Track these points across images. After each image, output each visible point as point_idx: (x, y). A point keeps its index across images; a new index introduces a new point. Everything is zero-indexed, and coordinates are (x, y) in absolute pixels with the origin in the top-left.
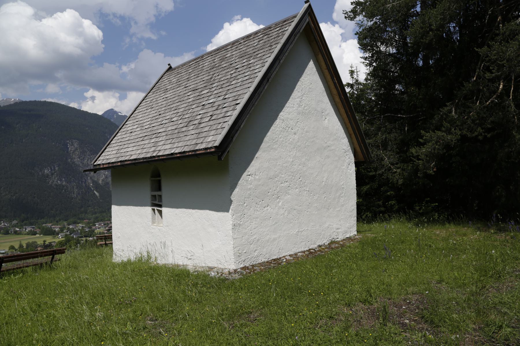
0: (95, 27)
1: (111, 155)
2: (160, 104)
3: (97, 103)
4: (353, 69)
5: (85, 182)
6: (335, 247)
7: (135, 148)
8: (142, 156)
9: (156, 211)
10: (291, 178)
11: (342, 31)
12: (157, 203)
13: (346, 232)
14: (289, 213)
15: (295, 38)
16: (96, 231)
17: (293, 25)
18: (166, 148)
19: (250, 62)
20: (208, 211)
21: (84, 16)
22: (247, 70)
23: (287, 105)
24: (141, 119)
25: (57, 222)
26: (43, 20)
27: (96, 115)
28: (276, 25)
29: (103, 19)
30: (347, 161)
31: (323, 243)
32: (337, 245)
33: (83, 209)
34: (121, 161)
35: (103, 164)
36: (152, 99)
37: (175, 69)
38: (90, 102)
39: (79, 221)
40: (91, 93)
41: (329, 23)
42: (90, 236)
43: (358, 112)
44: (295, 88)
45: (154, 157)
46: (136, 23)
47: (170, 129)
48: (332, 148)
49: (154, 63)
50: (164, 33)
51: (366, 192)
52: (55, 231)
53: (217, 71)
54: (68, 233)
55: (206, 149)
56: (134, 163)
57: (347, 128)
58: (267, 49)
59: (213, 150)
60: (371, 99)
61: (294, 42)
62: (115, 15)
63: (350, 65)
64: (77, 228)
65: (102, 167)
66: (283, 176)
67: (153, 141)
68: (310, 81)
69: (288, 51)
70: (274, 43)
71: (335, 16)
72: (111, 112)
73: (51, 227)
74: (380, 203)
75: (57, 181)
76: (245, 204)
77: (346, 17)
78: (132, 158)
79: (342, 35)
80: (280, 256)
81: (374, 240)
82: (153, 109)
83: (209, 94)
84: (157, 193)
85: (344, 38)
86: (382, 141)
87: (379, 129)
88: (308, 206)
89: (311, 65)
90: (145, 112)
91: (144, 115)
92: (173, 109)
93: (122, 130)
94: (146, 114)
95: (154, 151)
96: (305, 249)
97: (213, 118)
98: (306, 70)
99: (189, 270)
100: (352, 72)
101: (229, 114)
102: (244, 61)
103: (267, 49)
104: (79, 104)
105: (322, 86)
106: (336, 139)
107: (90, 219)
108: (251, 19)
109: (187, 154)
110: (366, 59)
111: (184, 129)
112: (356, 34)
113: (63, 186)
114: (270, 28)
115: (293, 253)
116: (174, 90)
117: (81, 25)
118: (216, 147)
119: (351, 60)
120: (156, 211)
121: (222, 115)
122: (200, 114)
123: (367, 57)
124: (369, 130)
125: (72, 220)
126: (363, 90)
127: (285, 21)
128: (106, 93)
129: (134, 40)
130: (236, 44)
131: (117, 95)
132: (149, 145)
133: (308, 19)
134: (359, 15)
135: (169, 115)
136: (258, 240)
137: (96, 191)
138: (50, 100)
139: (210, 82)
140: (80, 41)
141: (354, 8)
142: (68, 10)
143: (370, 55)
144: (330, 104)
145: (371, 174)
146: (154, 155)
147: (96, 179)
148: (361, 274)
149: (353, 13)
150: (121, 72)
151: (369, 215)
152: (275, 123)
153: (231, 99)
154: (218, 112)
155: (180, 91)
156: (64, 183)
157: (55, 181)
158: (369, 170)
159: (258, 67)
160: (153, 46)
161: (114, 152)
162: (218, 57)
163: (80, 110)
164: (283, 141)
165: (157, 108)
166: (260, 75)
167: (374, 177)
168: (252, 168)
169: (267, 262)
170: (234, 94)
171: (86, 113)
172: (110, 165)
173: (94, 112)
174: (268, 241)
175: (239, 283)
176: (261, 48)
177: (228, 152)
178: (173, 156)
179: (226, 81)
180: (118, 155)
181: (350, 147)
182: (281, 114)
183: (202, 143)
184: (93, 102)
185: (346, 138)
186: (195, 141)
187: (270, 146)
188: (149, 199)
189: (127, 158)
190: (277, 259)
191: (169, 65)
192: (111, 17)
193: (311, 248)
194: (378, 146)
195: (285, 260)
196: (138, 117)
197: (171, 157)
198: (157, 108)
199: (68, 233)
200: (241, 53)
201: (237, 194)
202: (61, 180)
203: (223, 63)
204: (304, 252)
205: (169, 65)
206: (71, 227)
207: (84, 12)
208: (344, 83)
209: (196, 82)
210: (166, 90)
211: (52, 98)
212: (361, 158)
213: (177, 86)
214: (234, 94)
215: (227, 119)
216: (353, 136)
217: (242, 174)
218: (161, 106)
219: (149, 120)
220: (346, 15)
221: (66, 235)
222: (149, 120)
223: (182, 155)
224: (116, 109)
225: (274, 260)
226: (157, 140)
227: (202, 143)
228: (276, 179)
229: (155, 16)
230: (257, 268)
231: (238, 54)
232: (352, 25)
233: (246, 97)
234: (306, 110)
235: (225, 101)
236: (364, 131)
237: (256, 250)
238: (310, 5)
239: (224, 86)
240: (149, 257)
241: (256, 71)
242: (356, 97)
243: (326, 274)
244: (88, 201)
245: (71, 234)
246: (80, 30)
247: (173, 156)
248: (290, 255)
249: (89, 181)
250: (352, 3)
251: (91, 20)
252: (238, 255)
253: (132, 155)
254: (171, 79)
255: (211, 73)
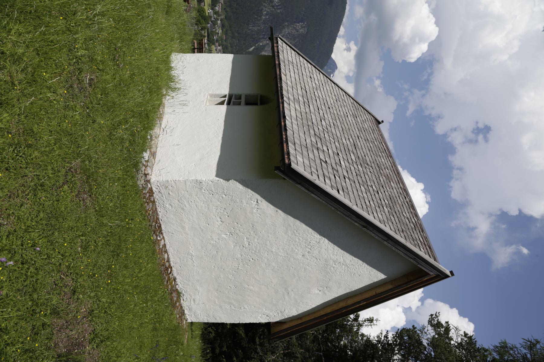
0: (420, 55)
1: (288, 55)
2: (340, 109)
3: (343, 54)
4: (375, 322)
5: (263, 38)
6: (172, 297)
7: (293, 79)
8: (284, 85)
9: (223, 99)
10: (253, 250)
11: (414, 309)
12: (232, 100)
13: (190, 309)
14: (213, 245)
15: (411, 258)
16: (213, 46)
17: (426, 257)
18: (291, 111)
19: (385, 208)
20: (219, 154)
21: (431, 45)
22: (376, 203)
23: (336, 247)
24: (325, 89)
25: (225, 9)
26: (427, 5)
27: (331, 51)
28: (426, 238)
29: (428, 63)
30: (271, 314)
31: (178, 283)
32: (175, 299)
33: (236, 34)
34: (279, 64)
35: (278, 47)
36: (346, 101)
37: (378, 127)
38: (344, 46)
39: (224, 30)
40: (354, 48)
41: (423, 295)
42: (208, 40)
43: (327, 326)
44: (355, 257)
45: (283, 98)
46: (423, 95)
47: (313, 117)
48: (287, 298)
49: (384, 109)
50: (412, 124)
51: (238, 333)
52: (216, 6)
53: (375, 171)
54: (213, 19)
55: (288, 154)
56: (276, 77)
57: (308, 315)
58: (399, 226)
59: (287, 161)
60: (341, 340)
61: (407, 258)
62: (431, 74)
63: (379, 319)
64: (217, 28)
65: (275, 45)
66: (256, 240)
67: (301, 98)
68: (363, 275)
69: (397, 250)
70: (406, 235)
71: (429, 301)
72: (334, 67)
73: (220, 3)
74: (225, 349)
75: (266, 11)
76: (224, 196)
77: (432, 315)
78: (283, 75)
79: (410, 308)
80: (164, 234)
81: (178, 343)
82: (335, 102)
83: (350, 161)
84: (243, 100)
85: (407, 310)
86: (293, 353)
87: (307, 350)
88: (221, 268)
89: (381, 276)
90: (333, 93)
91: (329, 92)
92: (335, 122)
93: (314, 68)
94: (330, 94)
95: (289, 99)
96: (171, 263)
97: (323, 163)
98: (375, 270)
99: (152, 129)
100: (371, 320)
101: (327, 181)
102: (386, 201)
103: (399, 226)
104: (343, 37)
105: (356, 288)
106: (296, 301)
107: (225, 41)
108: (427, 213)
109: (284, 133)
110: (386, 337)
111: (312, 132)
112: (413, 326)
113: (260, 16)
114: (422, 231)
115: (167, 248)
116: (355, 124)
117: (422, 40)
118: (290, 164)
119: (384, 320)
120: (223, 99)
121: (326, 173)
122: (335, 177)
123: (387, 338)
124: (307, 339)
125: (226, 23)
126: (351, 331)
127: (430, 248)
128: (354, 62)
129: (406, 94)
130: (405, 193)
131: (351, 74)
132: (296, 94)
133: (432, 274)
134: (435, 330)
135: (328, 117)
136: (183, 209)
137: (254, 49)
138: (348, 7)
139: (364, 163)
140: (406, 40)
141: (442, 325)
142: (437, 29)
143: (390, 342)
144: (337, 296)
145: (257, 339)
146: (285, 98)
147: (266, 49)
148: (134, 328)
149: (437, 324)
150: (374, 78)
151: (212, 335)
152: (316, 233)
153: (344, 184)
154: (330, 170)
155: (354, 130)
156: (264, 17)
157: (266, 9)
158: (262, 337)
159: (380, 216)
160: (400, 111)
161: (290, 59)
162: (391, 173)
163: (336, 36)
164: (296, 242)
165: (337, 106)
166: (370, 218)
167: (254, 343)
168: (264, 204)
169: (158, 219)
170: (350, 188)
171: (334, 42)
172: (276, 54)
173: (334, 50)
174: (182, 220)
175: (131, 184)
176: (401, 221)
177: (284, 179)
178: (282, 118)
179: (364, 180)
180: (287, 62)
181: (287, 317)
182: (326, 241)
183: (295, 150)
184: (345, 50)
185: (297, 314)
186: (299, 142)
187: (290, 226)
188: (236, 92)
189: (283, 70)
190: (161, 230)
191: (383, 121)
192: (429, 71)
193: (173, 269)
194: (288, 348)
195: (159, 238)
196: (327, 85)
197: (280, 116)
198: (337, 106)
199: (213, 19)
200: (395, 198)
201: (235, 186)
202: (266, 14)
203: (384, 178)
204: (168, 261)
205: (383, 121)
206: (219, 22)
207: (436, 45)
208: (359, 313)
209: (363, 148)
210: (355, 117)
211: (349, 11)
212: (274, 330)
213: (359, 128)
214: (350, 188)
215: (321, 178)
216: (300, 322)
217: (258, 194)
218: (338, 110)
219: (324, 96)
220: (434, 316)
221: (211, 17)
222: (324, 96)
223: (283, 128)
224: (337, 72)
225: (160, 227)
226: (302, 103)
227: (295, 150)
228: (252, 233)
229: (430, 115)
230: (151, 206)
231: (393, 194)
232: (423, 321)
233: (346, 201)
234: (330, 269)
235: (342, 177)
236: (305, 334)
237: (172, 206)
238: (448, 276)
239: (359, 178)
240: (174, 89)
241: (375, 214)
242: (343, 325)
243: (136, 287)
244: (244, 40)
245: (212, 22)
246: (417, 40)
247: (282, 118)
248: (165, 244)
249: (264, 42)
250: (447, 322)
251: (427, 51)
252: (166, 185)
253: (286, 75)
254: (367, 122)
255: (373, 165)
